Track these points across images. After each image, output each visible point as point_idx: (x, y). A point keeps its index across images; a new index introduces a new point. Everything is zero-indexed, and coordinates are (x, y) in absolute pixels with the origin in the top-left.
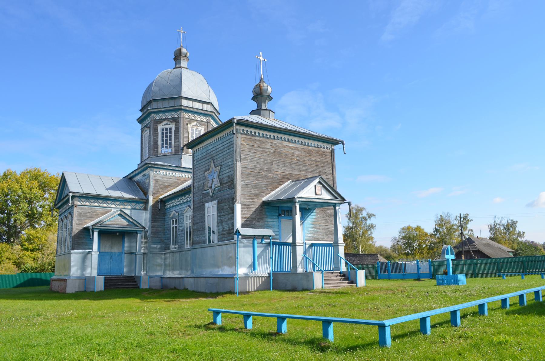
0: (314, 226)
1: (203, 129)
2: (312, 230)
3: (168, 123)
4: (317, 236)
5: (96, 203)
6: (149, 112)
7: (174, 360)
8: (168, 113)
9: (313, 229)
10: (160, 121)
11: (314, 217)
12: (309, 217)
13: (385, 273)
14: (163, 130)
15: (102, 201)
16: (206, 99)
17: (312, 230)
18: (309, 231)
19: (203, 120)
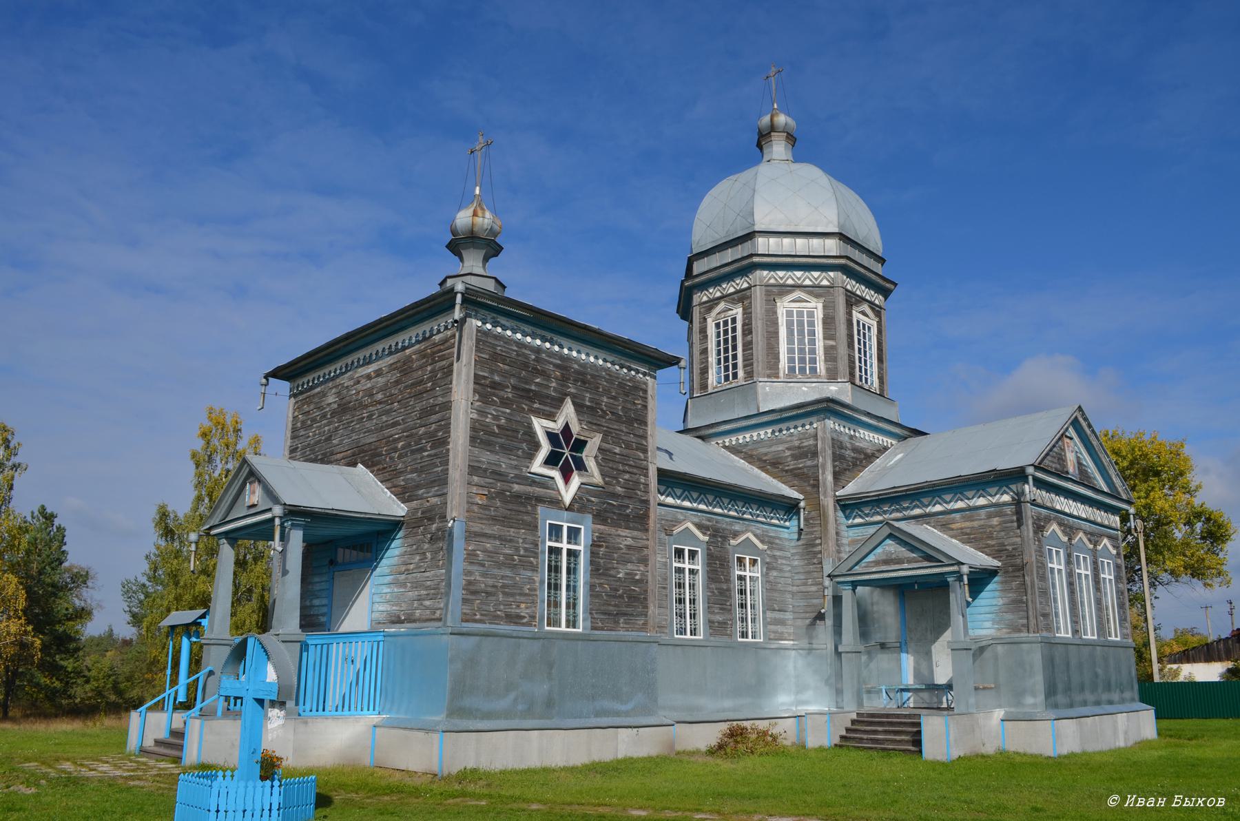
0: (393, 579)
1: (820, 306)
2: (388, 590)
3: (803, 296)
4: (397, 608)
5: (938, 506)
6: (752, 262)
7: (1101, 820)
8: (802, 271)
9: (389, 587)
10: (784, 289)
11: (397, 552)
12: (385, 556)
13: (348, 713)
14: (790, 313)
15: (975, 492)
16: (851, 235)
17: (388, 590)
18: (382, 597)
19: (786, 281)
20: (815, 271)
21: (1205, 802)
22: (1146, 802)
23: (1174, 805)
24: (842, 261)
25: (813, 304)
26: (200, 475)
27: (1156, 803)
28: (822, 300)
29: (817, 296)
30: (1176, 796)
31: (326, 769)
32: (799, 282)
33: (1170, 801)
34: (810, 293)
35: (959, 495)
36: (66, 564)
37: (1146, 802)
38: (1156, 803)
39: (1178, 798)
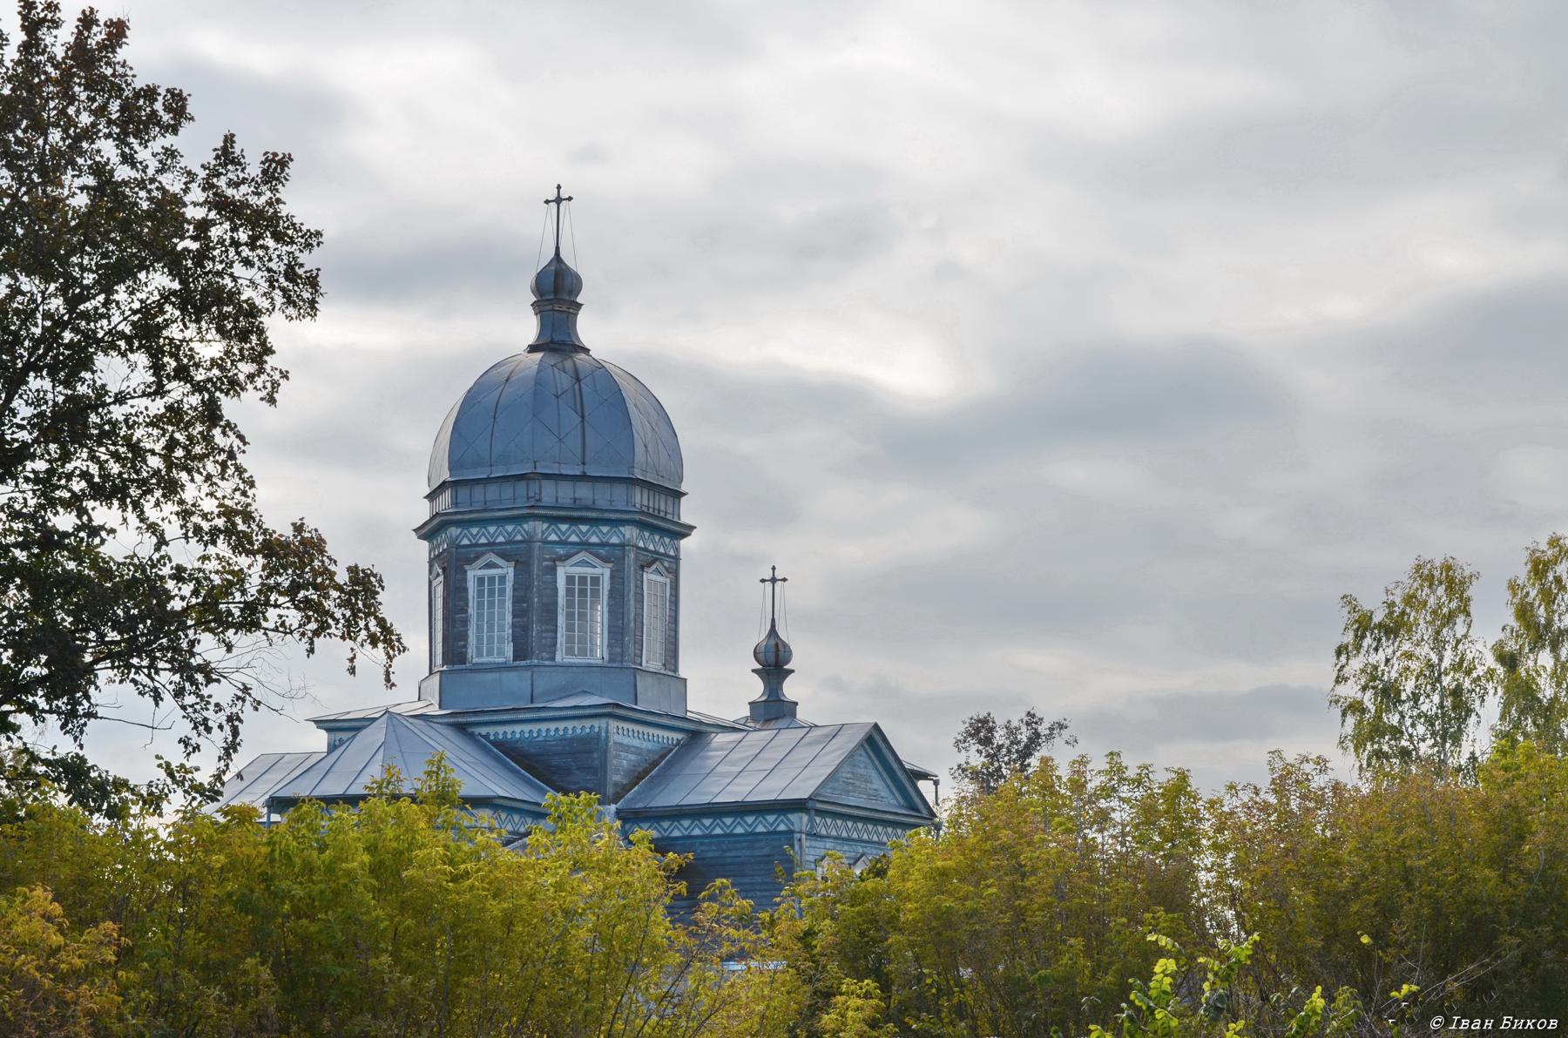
20: (603, 525)
21: (1534, 1024)
22: (1470, 1025)
23: (1502, 1027)
24: (438, 519)
25: (598, 571)
26: (304, 801)
27: (1482, 1025)
28: (611, 565)
29: (605, 560)
30: (1505, 1018)
31: (1324, 859)
32: (563, 538)
33: (1497, 1023)
34: (597, 556)
35: (718, 821)
36: (1548, 649)
37: (1470, 1025)
38: (1482, 1025)
39: (1508, 1020)
